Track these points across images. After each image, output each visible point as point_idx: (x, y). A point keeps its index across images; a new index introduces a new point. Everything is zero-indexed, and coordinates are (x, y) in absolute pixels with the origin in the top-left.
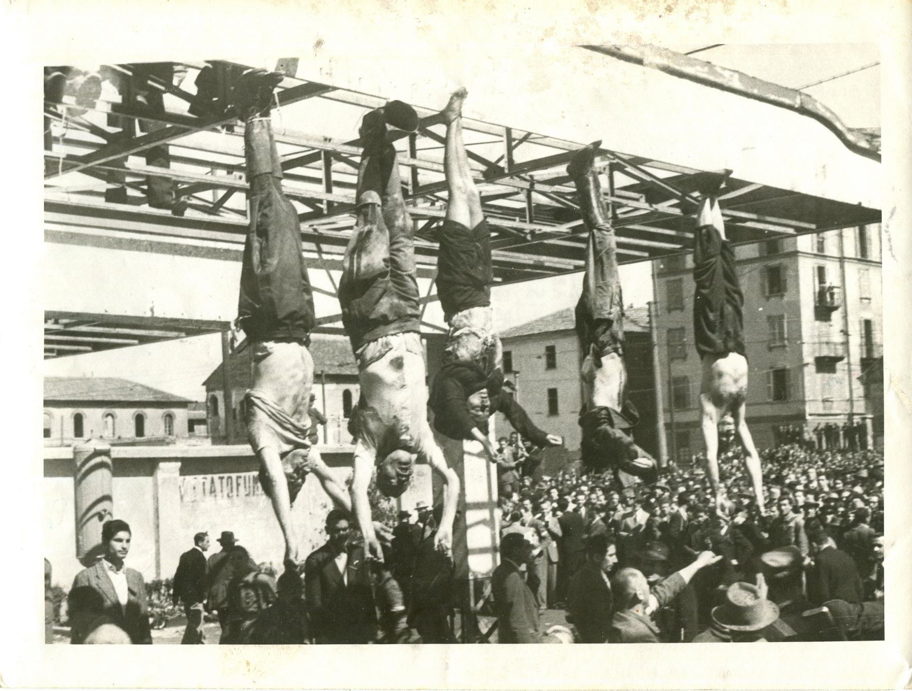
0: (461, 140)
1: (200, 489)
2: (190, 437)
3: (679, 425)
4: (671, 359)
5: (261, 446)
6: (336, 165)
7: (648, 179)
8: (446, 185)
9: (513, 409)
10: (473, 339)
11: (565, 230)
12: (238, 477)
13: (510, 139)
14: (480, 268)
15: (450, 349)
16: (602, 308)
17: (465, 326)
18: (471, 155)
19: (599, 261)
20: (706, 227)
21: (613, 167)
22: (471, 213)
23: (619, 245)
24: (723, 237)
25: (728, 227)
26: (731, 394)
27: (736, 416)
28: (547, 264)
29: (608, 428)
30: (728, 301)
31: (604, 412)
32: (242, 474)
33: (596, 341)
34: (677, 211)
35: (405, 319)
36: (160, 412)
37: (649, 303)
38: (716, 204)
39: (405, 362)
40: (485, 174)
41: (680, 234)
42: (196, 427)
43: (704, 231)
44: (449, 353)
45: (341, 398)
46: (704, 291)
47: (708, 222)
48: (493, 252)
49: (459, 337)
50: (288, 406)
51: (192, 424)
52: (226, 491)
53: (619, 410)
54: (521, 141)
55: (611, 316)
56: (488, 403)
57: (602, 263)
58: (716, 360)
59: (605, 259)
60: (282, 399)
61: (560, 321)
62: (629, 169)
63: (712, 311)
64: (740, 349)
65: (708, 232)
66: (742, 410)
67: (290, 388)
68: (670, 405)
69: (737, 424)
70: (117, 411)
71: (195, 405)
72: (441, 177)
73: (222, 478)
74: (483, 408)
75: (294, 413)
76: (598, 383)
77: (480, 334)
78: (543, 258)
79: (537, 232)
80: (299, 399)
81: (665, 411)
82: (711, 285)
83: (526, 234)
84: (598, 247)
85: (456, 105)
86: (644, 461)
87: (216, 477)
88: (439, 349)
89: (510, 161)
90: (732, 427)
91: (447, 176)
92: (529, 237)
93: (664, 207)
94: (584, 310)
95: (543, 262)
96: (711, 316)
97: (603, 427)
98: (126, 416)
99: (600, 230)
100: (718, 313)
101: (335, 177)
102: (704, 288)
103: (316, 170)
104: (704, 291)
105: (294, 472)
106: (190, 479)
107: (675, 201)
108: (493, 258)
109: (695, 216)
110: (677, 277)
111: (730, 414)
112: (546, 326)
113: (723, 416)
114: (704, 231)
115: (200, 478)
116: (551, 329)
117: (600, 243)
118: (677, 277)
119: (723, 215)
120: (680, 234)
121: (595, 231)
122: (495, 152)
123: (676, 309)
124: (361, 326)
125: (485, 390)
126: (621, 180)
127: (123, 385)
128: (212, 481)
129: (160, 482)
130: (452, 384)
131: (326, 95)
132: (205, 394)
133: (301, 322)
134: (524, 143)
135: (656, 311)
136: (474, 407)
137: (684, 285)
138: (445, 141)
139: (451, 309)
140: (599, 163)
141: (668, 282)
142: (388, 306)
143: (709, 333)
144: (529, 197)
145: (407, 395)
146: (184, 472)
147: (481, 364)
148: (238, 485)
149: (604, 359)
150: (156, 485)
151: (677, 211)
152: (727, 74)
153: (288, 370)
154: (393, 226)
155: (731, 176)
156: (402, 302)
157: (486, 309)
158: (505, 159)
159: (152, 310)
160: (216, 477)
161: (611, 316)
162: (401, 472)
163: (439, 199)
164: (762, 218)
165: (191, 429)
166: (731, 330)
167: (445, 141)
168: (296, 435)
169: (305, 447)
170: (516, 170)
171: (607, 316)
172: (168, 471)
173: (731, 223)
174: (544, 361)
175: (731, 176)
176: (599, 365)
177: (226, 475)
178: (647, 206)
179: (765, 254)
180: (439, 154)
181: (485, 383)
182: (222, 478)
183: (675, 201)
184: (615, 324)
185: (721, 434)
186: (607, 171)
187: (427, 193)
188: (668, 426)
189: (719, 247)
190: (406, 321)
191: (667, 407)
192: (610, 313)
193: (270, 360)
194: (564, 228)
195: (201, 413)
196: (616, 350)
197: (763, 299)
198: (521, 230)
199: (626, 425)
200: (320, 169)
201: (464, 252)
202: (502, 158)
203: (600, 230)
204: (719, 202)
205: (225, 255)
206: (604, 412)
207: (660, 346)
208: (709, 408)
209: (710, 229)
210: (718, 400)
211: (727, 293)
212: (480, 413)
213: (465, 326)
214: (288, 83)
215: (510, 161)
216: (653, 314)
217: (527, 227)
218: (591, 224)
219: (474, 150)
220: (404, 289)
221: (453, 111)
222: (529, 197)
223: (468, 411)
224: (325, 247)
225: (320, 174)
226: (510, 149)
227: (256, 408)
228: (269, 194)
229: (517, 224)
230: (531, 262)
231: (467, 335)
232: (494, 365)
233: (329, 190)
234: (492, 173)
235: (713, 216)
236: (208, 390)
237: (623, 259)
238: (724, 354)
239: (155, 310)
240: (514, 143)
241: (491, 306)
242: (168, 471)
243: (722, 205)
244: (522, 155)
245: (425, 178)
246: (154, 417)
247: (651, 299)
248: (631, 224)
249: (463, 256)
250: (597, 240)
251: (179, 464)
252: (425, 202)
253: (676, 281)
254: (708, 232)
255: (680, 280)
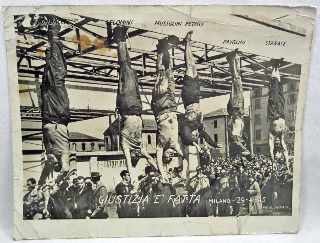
0: (190, 50)
1: (104, 164)
2: (99, 150)
3: (258, 145)
4: (255, 125)
5: (123, 148)
6: (147, 60)
7: (255, 63)
8: (185, 65)
9: (206, 136)
10: (193, 113)
11: (225, 80)
12: (115, 161)
13: (207, 49)
14: (196, 91)
15: (186, 117)
16: (235, 104)
17: (191, 109)
18: (194, 55)
19: (235, 89)
20: (273, 77)
21: (241, 59)
22: (193, 73)
23: (243, 85)
24: (280, 81)
25: (281, 78)
26: (279, 131)
27: (280, 138)
28: (217, 92)
29: (237, 142)
30: (279, 102)
31: (235, 137)
32: (117, 161)
33: (233, 114)
34: (263, 73)
35: (173, 108)
36: (90, 142)
37: (249, 106)
38: (278, 70)
39: (173, 121)
40: (198, 61)
41: (263, 81)
42: (101, 147)
43: (273, 79)
44: (186, 118)
45: (147, 138)
46: (271, 99)
47: (274, 76)
48: (201, 88)
49: (189, 113)
50: (133, 136)
51: (100, 146)
52: (112, 165)
53: (241, 136)
54: (210, 50)
55: (239, 106)
56: (198, 134)
57: (236, 89)
58: (274, 120)
59: (237, 88)
60: (131, 133)
61: (219, 113)
62: (248, 59)
63: (274, 105)
64: (283, 117)
65: (274, 80)
66: (283, 137)
67: (133, 130)
68: (255, 139)
69: (281, 141)
70: (77, 143)
71: (101, 140)
72: (184, 62)
73: (110, 162)
74: (196, 135)
75: (135, 138)
76: (234, 128)
77: (196, 112)
78: (215, 90)
79: (214, 81)
80: (137, 133)
81: (253, 141)
82: (274, 96)
83: (210, 82)
84: (235, 84)
85: (189, 36)
86: (246, 153)
87: (109, 161)
88: (181, 117)
89: (207, 57)
90: (279, 142)
91: (185, 62)
92: (211, 83)
93: (259, 72)
94: (230, 105)
95: (216, 91)
96: (273, 106)
97: (235, 142)
98: (79, 144)
99: (236, 78)
100: (276, 105)
101: (147, 64)
102: (272, 97)
103: (140, 62)
104: (271, 99)
105: (135, 156)
106: (101, 162)
107: (263, 70)
108: (201, 90)
109: (270, 75)
110: (259, 98)
111: (278, 137)
112: (215, 114)
113: (276, 138)
114: (273, 79)
115: (104, 162)
116: (216, 115)
117: (236, 83)
118: (259, 98)
119: (280, 74)
120: (263, 81)
121: (234, 79)
122: (201, 54)
123: (258, 108)
124: (157, 110)
125: (197, 130)
126: (244, 63)
127: (78, 134)
128: (108, 163)
129: (91, 163)
130: (187, 129)
131: (143, 34)
132: (104, 137)
133: (137, 109)
134: (211, 51)
135: (252, 108)
136: (193, 135)
137: (261, 101)
138: (184, 51)
139: (186, 103)
140: (238, 57)
141: (256, 100)
142: (167, 103)
143: (272, 112)
144: (212, 69)
145: (171, 132)
146: (98, 160)
147: (196, 122)
148: (116, 164)
149: (236, 120)
150: (90, 163)
151: (263, 73)
152: (285, 25)
153: (132, 124)
154: (169, 77)
155: (284, 60)
156: (171, 102)
157: (198, 104)
158: (205, 56)
159: (88, 107)
160: (109, 161)
161: (239, 106)
162: (170, 155)
163: (181, 70)
164: (292, 75)
165: (100, 148)
166: (280, 111)
167: (184, 51)
168: (136, 145)
169: (139, 148)
170: (209, 59)
171: (237, 106)
172: (94, 160)
173: (282, 77)
174: (213, 125)
175: (284, 60)
176: (234, 122)
177: (112, 161)
178: (253, 71)
179: (289, 90)
180: (183, 55)
181: (197, 128)
182: (110, 162)
183: (263, 70)
184: (240, 109)
185: (275, 144)
186: (239, 60)
187: (177, 68)
188: (254, 145)
189: (278, 84)
190: (172, 108)
191: (254, 139)
192: (238, 105)
193: (127, 121)
194: (224, 79)
195: (103, 143)
196: (240, 117)
197: (288, 105)
198: (209, 80)
199: (243, 141)
200: (142, 61)
201: (191, 85)
202: (204, 55)
203: (236, 78)
204: (279, 70)
205: (110, 91)
206: (235, 137)
207: (252, 119)
208: (271, 136)
209: (275, 78)
210: (274, 133)
211: (279, 98)
212: (196, 137)
213: (191, 109)
214: (130, 30)
215: (207, 57)
216: (250, 109)
217: (211, 79)
218: (234, 77)
219: (195, 53)
220: (172, 97)
221: (188, 38)
222: (212, 69)
223: (191, 136)
224: (143, 87)
225: (142, 63)
226: (207, 52)
227: (122, 136)
228: (125, 68)
229: (207, 78)
230: (212, 91)
231: (192, 112)
232: (200, 122)
233: (145, 68)
234: (200, 61)
235: (276, 74)
236: (105, 136)
237: (244, 90)
238: (277, 119)
239: (89, 107)
240: (208, 51)
241: (200, 103)
242: (94, 160)
243: (280, 71)
244: (211, 54)
245: (177, 63)
246: (88, 144)
247: (250, 105)
248: (248, 77)
249: (191, 87)
250: (235, 82)
251: (97, 158)
252: (177, 71)
253: (258, 99)
254: (274, 80)
255: (260, 99)
